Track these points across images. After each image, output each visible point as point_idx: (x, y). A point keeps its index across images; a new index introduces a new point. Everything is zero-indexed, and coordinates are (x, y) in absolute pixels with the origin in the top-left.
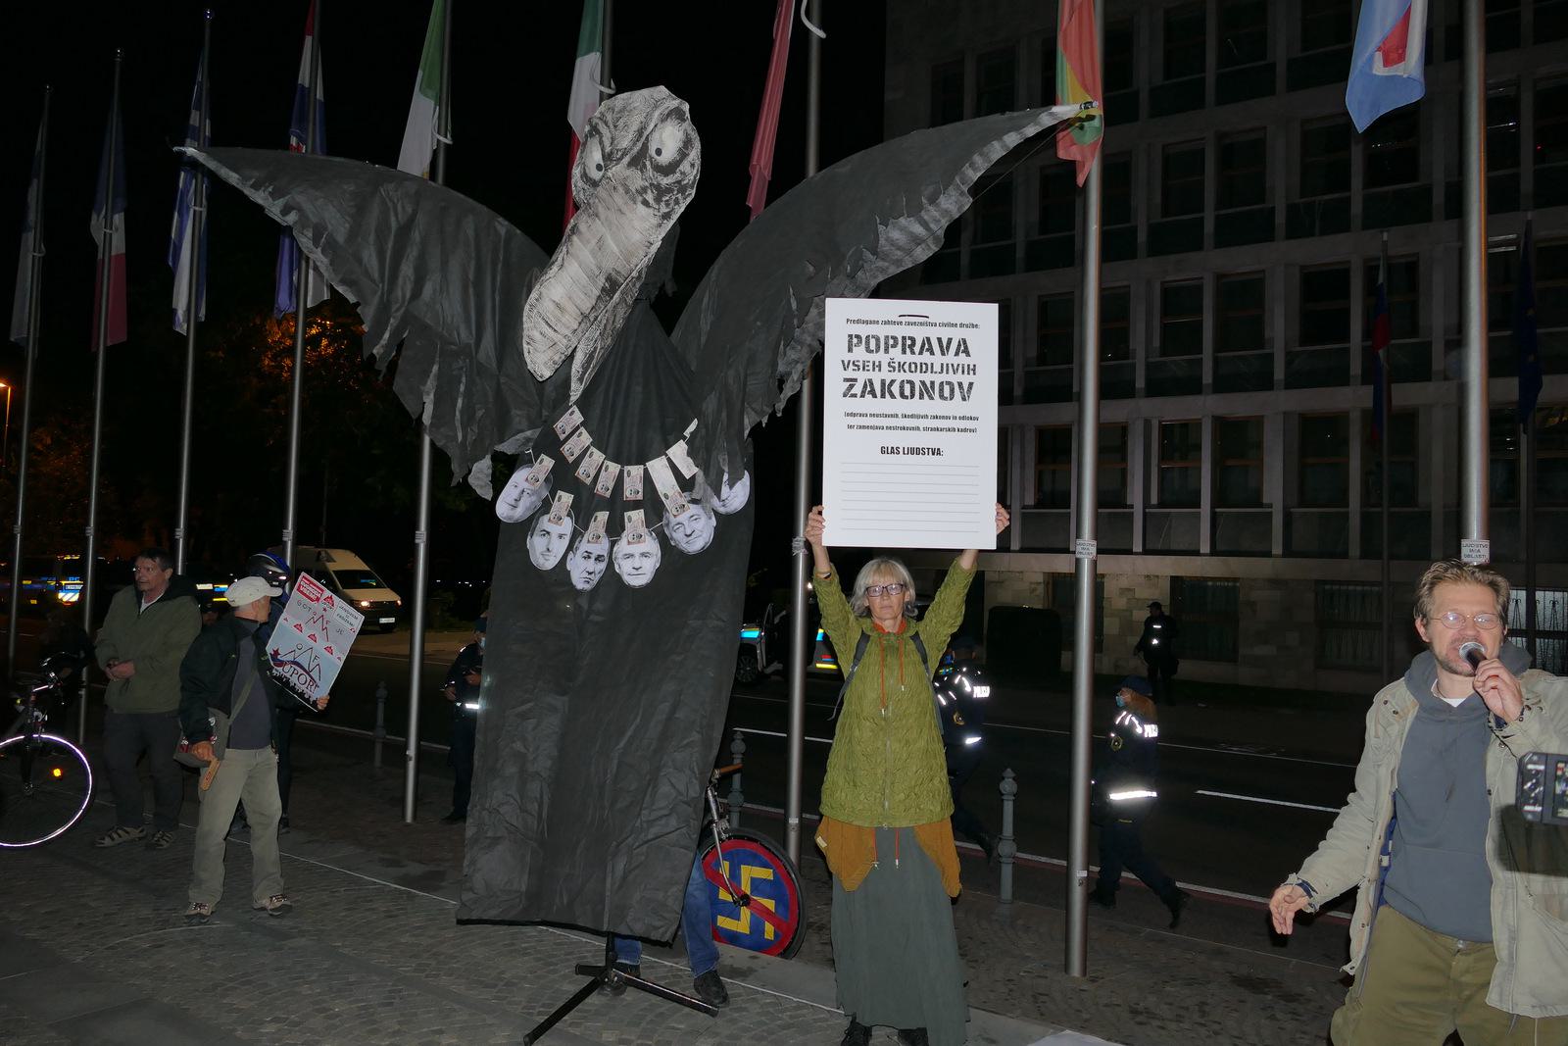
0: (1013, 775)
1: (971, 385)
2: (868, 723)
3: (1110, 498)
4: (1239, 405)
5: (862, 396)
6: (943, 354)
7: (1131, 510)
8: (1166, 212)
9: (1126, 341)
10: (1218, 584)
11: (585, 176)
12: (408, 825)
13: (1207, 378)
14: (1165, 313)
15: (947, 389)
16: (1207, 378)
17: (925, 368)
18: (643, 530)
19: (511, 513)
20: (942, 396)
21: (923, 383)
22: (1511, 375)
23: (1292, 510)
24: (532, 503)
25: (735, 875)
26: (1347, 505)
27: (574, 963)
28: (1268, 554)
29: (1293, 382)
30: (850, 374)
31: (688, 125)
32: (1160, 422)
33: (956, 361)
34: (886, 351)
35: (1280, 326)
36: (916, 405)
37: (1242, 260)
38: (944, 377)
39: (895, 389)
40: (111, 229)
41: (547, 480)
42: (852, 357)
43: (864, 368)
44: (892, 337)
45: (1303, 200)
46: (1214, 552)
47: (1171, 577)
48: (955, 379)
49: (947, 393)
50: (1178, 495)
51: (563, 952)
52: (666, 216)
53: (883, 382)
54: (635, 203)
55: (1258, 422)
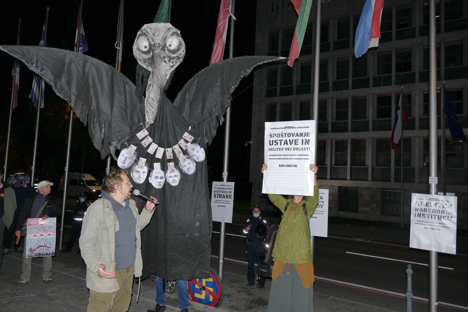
1: (323, 205)
4: (359, 135)
8: (338, 78)
9: (326, 116)
11: (138, 49)
13: (350, 127)
14: (337, 108)
18: (174, 168)
19: (123, 165)
23: (374, 167)
24: (130, 162)
25: (201, 281)
26: (390, 166)
28: (367, 180)
35: (371, 113)
37: (360, 92)
40: (16, 73)
45: (378, 76)
46: (351, 179)
47: (338, 186)
50: (340, 162)
52: (172, 66)
54: (162, 62)
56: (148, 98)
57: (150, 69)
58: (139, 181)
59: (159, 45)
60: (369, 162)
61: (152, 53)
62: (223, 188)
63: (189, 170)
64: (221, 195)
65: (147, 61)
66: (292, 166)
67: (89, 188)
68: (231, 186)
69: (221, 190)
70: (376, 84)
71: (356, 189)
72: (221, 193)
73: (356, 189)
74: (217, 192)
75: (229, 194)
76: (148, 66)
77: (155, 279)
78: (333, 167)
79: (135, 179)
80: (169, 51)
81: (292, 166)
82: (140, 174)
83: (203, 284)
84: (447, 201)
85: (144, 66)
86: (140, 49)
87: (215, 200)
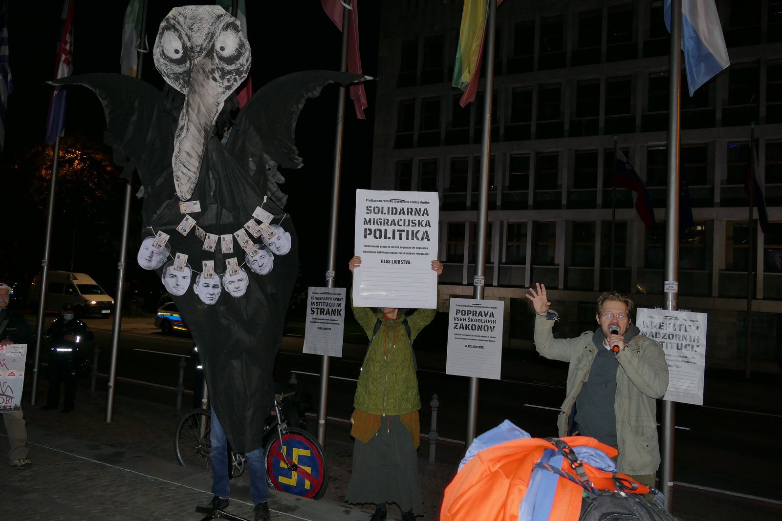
0: (437, 397)
3: (488, 272)
4: (545, 216)
7: (492, 265)
11: (163, 55)
12: (108, 424)
13: (531, 202)
15: (486, 327)
16: (531, 202)
17: (479, 321)
18: (238, 268)
19: (149, 264)
20: (484, 330)
21: (479, 325)
23: (568, 267)
25: (290, 454)
27: (196, 505)
29: (570, 206)
30: (456, 322)
31: (243, 35)
32: (508, 222)
33: (489, 319)
34: (468, 315)
35: (565, 178)
36: (476, 332)
37: (548, 146)
38: (485, 324)
39: (470, 327)
41: (166, 246)
42: (457, 316)
44: (410, 209)
48: (488, 324)
49: (486, 329)
51: (190, 499)
52: (228, 88)
53: (466, 325)
54: (208, 79)
55: (553, 225)
56: (178, 153)
57: (185, 91)
58: (176, 291)
59: (201, 49)
60: (560, 257)
61: (188, 62)
62: (327, 299)
63: (262, 267)
64: (324, 309)
65: (181, 77)
66: (403, 262)
67: (83, 297)
68: (340, 294)
69: (323, 301)
70: (576, 131)
72: (323, 307)
74: (316, 304)
75: (337, 308)
76: (184, 87)
77: (208, 453)
80: (221, 58)
81: (403, 262)
82: (177, 279)
83: (294, 461)
84: (691, 321)
85: (176, 86)
86: (167, 54)
87: (313, 319)
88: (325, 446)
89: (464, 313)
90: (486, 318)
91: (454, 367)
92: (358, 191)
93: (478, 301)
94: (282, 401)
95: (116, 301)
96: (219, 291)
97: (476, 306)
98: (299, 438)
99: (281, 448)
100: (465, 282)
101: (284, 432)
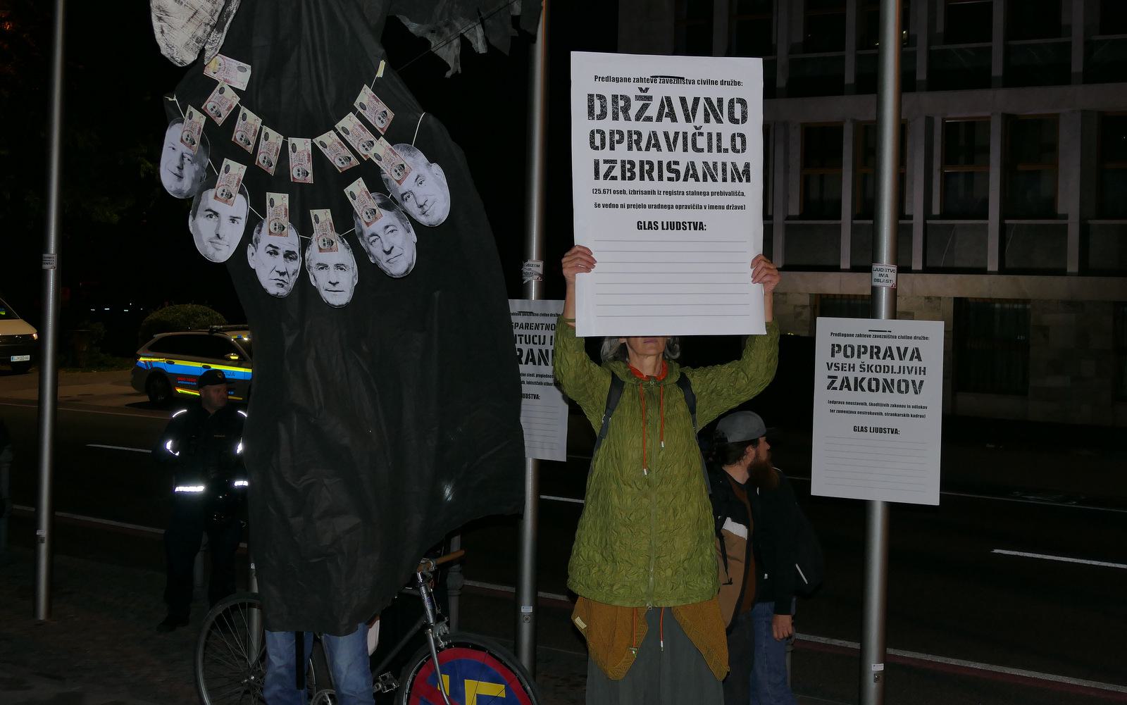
1: (922, 382)
2: (629, 489)
4: (1032, 102)
5: (841, 389)
6: (901, 359)
7: (910, 222)
10: (1007, 306)
12: (42, 623)
13: (997, 71)
15: (903, 385)
16: (997, 71)
17: (887, 369)
18: (334, 236)
20: (899, 391)
21: (885, 380)
22: (947, 482)
24: (196, 172)
28: (1062, 272)
29: (1092, 76)
30: (832, 373)
32: (943, 120)
34: (859, 356)
36: (879, 397)
38: (901, 376)
39: (865, 384)
42: (834, 360)
43: (842, 370)
46: (1003, 270)
47: (955, 298)
49: (903, 388)
50: (961, 204)
53: (856, 379)
60: (1069, 201)
71: (1020, 306)
73: (1020, 306)
78: (934, 226)
79: (201, 241)
81: (687, 225)
82: (219, 222)
88: (535, 673)
89: (849, 351)
90: (902, 363)
91: (830, 478)
92: (574, 54)
93: (883, 321)
94: (435, 573)
95: (42, 333)
96: (296, 267)
97: (878, 333)
98: (479, 657)
99: (436, 680)
100: (845, 263)
101: (442, 644)
